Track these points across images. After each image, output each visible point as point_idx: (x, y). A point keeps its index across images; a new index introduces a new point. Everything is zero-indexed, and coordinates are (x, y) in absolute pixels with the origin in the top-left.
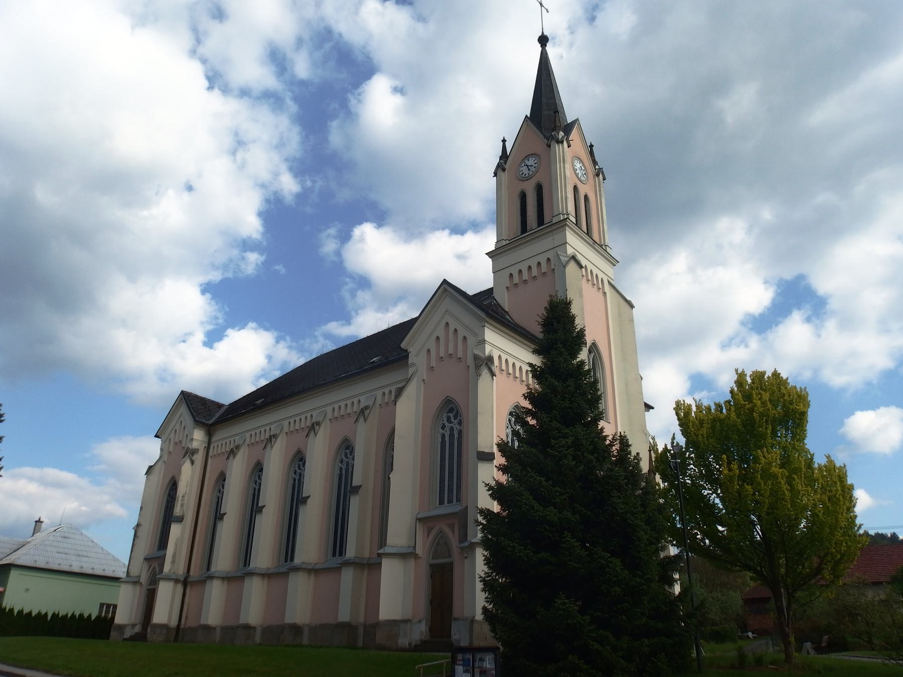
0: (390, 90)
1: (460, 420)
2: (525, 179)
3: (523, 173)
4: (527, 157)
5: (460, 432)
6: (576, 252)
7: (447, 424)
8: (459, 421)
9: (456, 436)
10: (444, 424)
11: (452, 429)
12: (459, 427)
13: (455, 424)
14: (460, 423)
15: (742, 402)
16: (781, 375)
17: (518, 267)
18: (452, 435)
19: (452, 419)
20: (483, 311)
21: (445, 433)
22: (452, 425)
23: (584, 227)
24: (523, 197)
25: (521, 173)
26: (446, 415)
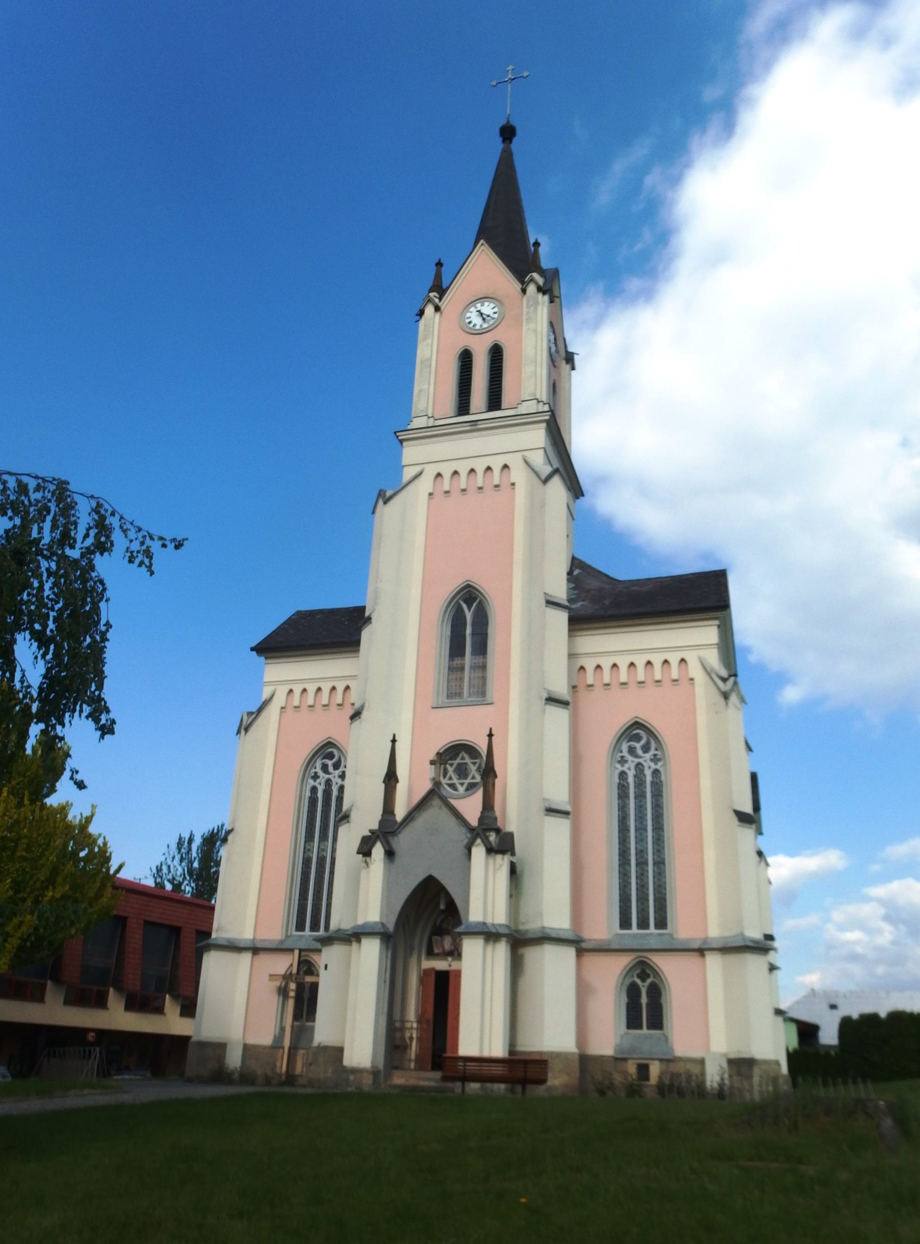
0: (828, 1007)
1: (344, 772)
2: (474, 332)
3: (470, 323)
4: (483, 299)
5: (341, 789)
6: (462, 700)
7: (321, 773)
8: (341, 774)
9: (335, 793)
10: (316, 773)
11: (328, 783)
12: (340, 781)
13: (334, 777)
14: (343, 776)
15: (89, 605)
16: (107, 643)
17: (454, 466)
18: (327, 793)
19: (331, 769)
20: (696, 719)
21: (318, 786)
22: (330, 776)
23: (290, 969)
24: (466, 359)
25: (468, 321)
26: (320, 762)
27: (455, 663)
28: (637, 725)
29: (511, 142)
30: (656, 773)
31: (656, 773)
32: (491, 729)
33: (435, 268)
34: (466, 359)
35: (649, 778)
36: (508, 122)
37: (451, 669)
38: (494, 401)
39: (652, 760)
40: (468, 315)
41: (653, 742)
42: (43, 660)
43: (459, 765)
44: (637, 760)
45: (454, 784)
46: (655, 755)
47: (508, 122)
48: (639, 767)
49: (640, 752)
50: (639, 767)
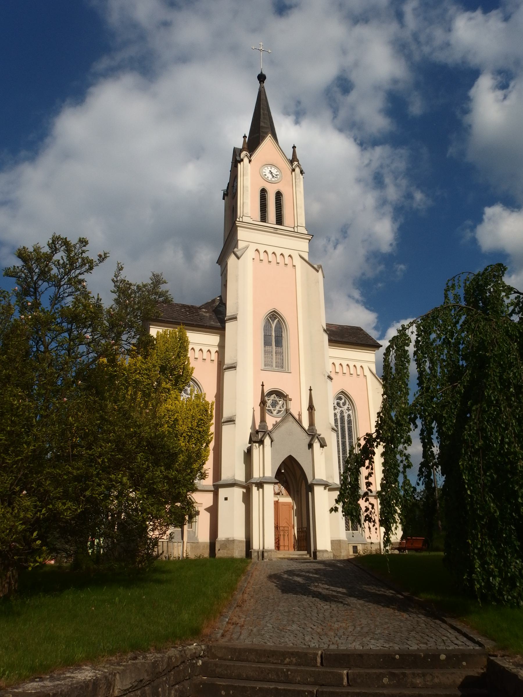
4: (272, 165)
25: (264, 174)
27: (267, 348)
28: (343, 392)
29: (264, 83)
30: (349, 416)
31: (349, 416)
32: (310, 387)
33: (292, 149)
34: (263, 192)
35: (346, 418)
36: (261, 72)
37: (265, 351)
38: (279, 220)
39: (347, 409)
40: (266, 168)
41: (347, 401)
42: (416, 336)
43: (276, 401)
44: (341, 409)
45: (271, 410)
46: (348, 407)
47: (261, 72)
48: (342, 412)
49: (341, 405)
50: (342, 412)
